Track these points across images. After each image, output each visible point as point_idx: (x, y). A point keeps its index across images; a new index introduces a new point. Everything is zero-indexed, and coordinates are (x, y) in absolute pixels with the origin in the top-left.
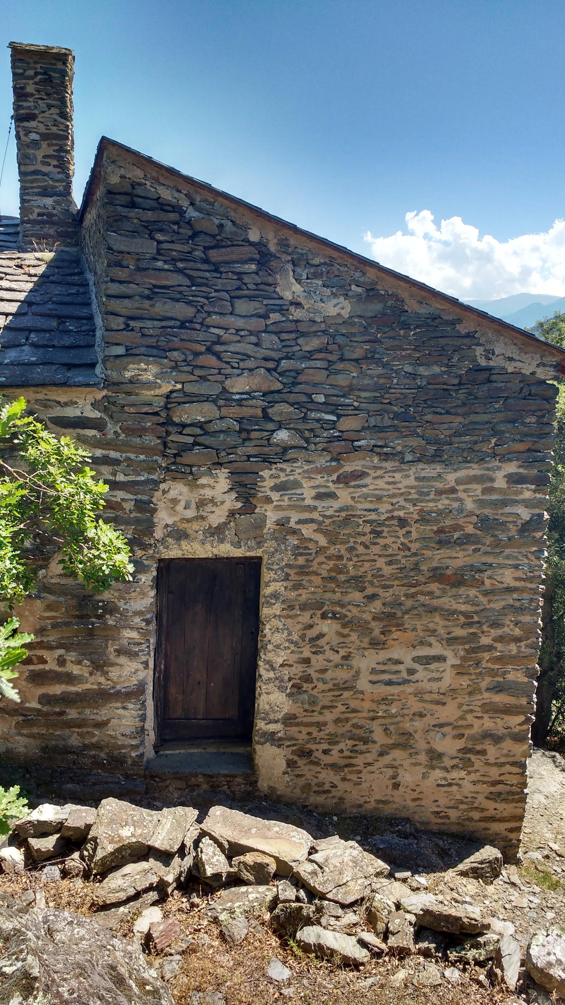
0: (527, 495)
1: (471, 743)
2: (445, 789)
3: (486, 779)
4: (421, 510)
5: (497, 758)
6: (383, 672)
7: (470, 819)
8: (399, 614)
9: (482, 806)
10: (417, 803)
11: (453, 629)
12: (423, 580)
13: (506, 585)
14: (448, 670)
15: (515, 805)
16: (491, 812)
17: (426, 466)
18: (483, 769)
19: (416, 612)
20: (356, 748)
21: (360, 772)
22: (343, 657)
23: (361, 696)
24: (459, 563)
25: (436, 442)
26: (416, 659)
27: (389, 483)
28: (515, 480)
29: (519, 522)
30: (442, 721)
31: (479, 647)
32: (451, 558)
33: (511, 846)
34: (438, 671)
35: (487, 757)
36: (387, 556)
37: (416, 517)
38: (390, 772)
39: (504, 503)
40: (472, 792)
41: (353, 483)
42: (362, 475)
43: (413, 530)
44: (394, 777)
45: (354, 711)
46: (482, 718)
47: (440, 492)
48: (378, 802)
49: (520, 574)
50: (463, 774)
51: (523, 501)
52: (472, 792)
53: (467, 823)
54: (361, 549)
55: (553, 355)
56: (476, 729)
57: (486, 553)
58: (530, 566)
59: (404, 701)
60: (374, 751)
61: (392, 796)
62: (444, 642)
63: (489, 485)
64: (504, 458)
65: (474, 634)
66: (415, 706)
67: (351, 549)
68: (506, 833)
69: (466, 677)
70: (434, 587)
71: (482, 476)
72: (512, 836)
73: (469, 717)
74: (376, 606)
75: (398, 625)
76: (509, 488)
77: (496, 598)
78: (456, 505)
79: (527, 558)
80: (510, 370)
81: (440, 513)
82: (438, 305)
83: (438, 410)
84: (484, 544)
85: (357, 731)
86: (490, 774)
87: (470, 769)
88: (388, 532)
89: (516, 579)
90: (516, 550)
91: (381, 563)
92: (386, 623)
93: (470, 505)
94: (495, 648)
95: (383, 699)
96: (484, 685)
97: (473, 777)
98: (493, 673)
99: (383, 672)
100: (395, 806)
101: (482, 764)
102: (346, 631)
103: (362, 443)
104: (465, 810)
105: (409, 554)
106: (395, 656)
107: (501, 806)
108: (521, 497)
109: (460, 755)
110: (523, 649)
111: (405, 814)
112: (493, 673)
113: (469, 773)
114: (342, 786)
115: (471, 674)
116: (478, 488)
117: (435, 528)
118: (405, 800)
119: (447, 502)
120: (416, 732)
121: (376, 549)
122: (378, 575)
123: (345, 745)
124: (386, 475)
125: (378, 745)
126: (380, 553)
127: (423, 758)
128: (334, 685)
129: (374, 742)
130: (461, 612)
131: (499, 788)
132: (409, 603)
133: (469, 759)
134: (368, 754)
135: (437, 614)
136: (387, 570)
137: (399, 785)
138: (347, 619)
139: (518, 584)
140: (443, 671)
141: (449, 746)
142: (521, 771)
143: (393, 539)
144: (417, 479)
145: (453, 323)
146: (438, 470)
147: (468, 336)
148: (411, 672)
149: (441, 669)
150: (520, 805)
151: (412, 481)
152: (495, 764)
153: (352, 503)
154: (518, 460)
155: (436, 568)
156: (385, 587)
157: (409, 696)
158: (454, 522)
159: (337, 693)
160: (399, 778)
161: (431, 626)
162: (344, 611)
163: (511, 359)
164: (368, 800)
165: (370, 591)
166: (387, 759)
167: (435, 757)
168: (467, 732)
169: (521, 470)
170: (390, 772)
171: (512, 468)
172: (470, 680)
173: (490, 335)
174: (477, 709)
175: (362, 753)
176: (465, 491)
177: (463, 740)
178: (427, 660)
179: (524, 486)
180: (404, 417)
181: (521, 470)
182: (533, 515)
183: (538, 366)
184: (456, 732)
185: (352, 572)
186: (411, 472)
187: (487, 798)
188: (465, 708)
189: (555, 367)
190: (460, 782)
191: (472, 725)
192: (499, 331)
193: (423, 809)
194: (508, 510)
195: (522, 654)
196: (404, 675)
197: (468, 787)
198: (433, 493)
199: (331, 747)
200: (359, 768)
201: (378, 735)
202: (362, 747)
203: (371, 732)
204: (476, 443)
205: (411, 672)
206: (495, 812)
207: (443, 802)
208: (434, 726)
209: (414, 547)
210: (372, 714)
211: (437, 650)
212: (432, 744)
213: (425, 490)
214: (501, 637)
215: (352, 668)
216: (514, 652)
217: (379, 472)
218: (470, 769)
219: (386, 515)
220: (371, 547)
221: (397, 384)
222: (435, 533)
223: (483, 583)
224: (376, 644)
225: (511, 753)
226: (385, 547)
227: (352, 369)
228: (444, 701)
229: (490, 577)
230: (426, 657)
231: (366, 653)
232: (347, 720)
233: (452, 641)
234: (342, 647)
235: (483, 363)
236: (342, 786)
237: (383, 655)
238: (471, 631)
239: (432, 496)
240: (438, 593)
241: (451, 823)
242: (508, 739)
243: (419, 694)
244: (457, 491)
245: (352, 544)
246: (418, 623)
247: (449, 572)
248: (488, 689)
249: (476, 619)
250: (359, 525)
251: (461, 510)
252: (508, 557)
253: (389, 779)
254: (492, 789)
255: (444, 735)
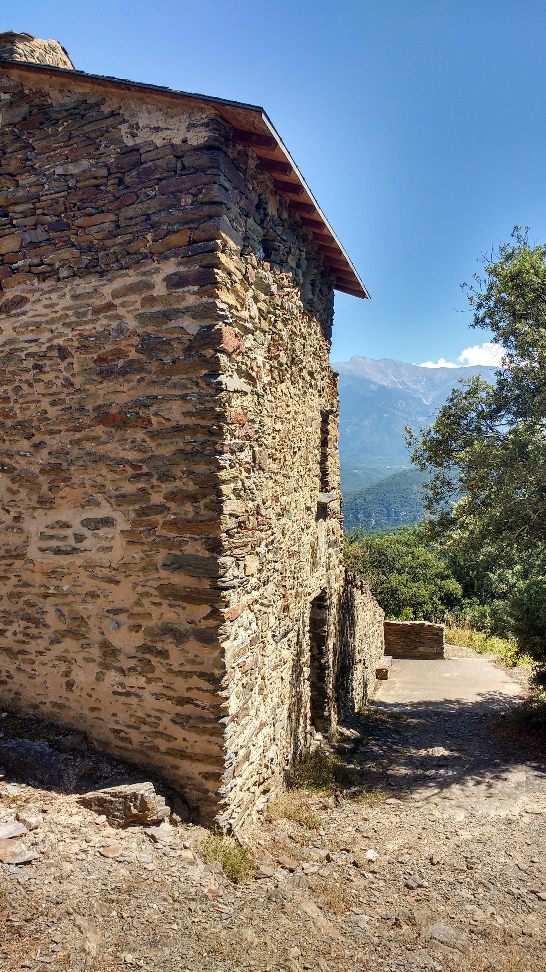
0: (191, 300)
1: (149, 638)
2: (122, 699)
3: (170, 693)
4: (81, 335)
5: (181, 665)
6: (52, 537)
7: (156, 749)
8: (65, 466)
9: (168, 732)
10: (95, 714)
11: (121, 484)
12: (88, 422)
13: (174, 424)
14: (118, 537)
15: (207, 737)
16: (179, 744)
17: (82, 281)
18: (168, 678)
19: (81, 462)
20: (28, 631)
21: (33, 662)
22: (14, 518)
23: (31, 566)
24: (123, 399)
25: (91, 248)
26: (85, 523)
27: (46, 307)
28: (175, 282)
29: (185, 338)
30: (117, 605)
31: (150, 508)
32: (114, 392)
33: (206, 800)
34: (107, 538)
35: (169, 662)
36: (50, 394)
37: (76, 344)
38: (63, 667)
39: (167, 316)
40: (156, 710)
41: (13, 312)
42: (21, 301)
43: (75, 360)
44: (67, 674)
45: (26, 585)
46: (160, 604)
47: (97, 311)
48: (54, 704)
49: (189, 408)
50: (142, 681)
51: (187, 310)
52: (156, 710)
53: (151, 753)
54: (25, 387)
55: (201, 110)
56: (153, 622)
57: (153, 383)
58: (200, 396)
59: (74, 575)
60: (46, 637)
61: (67, 699)
62: (112, 501)
63: (148, 293)
64: (163, 257)
65: (143, 490)
66: (90, 585)
67: (17, 389)
68: (199, 778)
69: (139, 548)
70: (100, 430)
71: (138, 284)
72: (209, 785)
73: (146, 601)
74: (43, 457)
75: (65, 480)
76: (169, 294)
77: (165, 441)
78: (114, 324)
79: (197, 384)
80: (159, 142)
81: (99, 336)
82: (82, 90)
83: (87, 211)
84: (149, 372)
85: (30, 611)
86: (174, 686)
87: (150, 675)
88: (51, 365)
89: (187, 414)
90: (184, 376)
91: (45, 403)
92: (54, 477)
93: (131, 323)
94: (168, 509)
95: (53, 572)
96: (161, 557)
97: (156, 687)
98: (168, 543)
99: (52, 537)
100: (72, 713)
101: (165, 671)
102: (15, 487)
103: (20, 263)
104: (148, 734)
105: (71, 390)
106: (64, 518)
107: (192, 736)
108: (184, 304)
109: (139, 655)
110: (202, 512)
111: (82, 726)
112: (168, 543)
113: (149, 681)
114: (19, 678)
115: (142, 543)
116: (136, 299)
117: (95, 356)
118: (82, 708)
119: (105, 322)
120: (89, 617)
121: (40, 388)
122: (43, 416)
123: (18, 625)
124: (43, 298)
125: (51, 631)
126: (44, 392)
127: (95, 652)
128: (6, 551)
129: (46, 626)
130: (128, 461)
131: (188, 709)
132: (75, 452)
133: (149, 661)
134: (39, 641)
135: (102, 464)
136: (53, 412)
137: (72, 685)
138: (16, 473)
139: (188, 421)
140: (113, 538)
141: (126, 640)
142: (212, 687)
143: (55, 374)
144: (75, 297)
145: (97, 105)
146: (94, 284)
147: (113, 114)
148: (79, 538)
149: (110, 536)
150: (214, 739)
151: (68, 301)
152: (179, 673)
153: (14, 335)
154: (176, 255)
155: (100, 406)
156: (51, 433)
157: (79, 570)
158: (115, 347)
159: (9, 561)
160: (73, 676)
161: (99, 480)
162: (12, 463)
163: (157, 129)
164: (44, 701)
165: (37, 439)
166: (58, 650)
167: (109, 651)
168: (145, 623)
169: (181, 269)
170: (63, 667)
171: (170, 267)
172: (143, 551)
173: (133, 107)
174: (154, 592)
175: (33, 638)
176: (123, 305)
177: (141, 633)
178: (95, 524)
179: (186, 289)
180: (60, 227)
181: (181, 269)
182: (202, 327)
183: (188, 129)
184: (131, 622)
185: (20, 417)
186: (67, 290)
187: (173, 721)
188: (140, 589)
189: (207, 125)
190: (140, 692)
191: (150, 615)
192: (141, 99)
193: (101, 723)
194: (172, 324)
195: (200, 518)
196: (72, 541)
197: (150, 703)
198: (90, 312)
199: (6, 628)
200: (32, 657)
201: (51, 618)
202: (33, 631)
203: (44, 612)
204: (130, 242)
205: (79, 538)
206: (184, 744)
207: (123, 717)
208: (108, 611)
209: (78, 381)
210: (43, 590)
211: (105, 511)
212: (106, 636)
213: (82, 310)
214: (172, 493)
215: (22, 531)
216: (191, 515)
217: (37, 295)
218: (150, 675)
219: (47, 345)
220: (35, 384)
221: (49, 190)
222: (95, 362)
223: (150, 422)
224: (45, 503)
225: (198, 660)
226: (49, 384)
227: (9, 184)
228: (117, 578)
229: (156, 414)
230: (95, 520)
231: (36, 514)
232: (19, 595)
233: (122, 499)
234: (12, 506)
235: (130, 142)
236: (19, 678)
237: (52, 517)
238: (141, 485)
239: (90, 317)
240: (104, 438)
241: (133, 750)
242: (192, 638)
243: (89, 566)
244: (113, 305)
245: (17, 384)
246: (86, 477)
247: (114, 410)
248: (165, 566)
249: (145, 470)
250: (21, 360)
251: (120, 331)
252: (174, 386)
253: (62, 676)
254: (179, 709)
255: (119, 625)
